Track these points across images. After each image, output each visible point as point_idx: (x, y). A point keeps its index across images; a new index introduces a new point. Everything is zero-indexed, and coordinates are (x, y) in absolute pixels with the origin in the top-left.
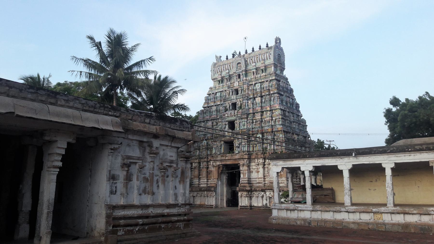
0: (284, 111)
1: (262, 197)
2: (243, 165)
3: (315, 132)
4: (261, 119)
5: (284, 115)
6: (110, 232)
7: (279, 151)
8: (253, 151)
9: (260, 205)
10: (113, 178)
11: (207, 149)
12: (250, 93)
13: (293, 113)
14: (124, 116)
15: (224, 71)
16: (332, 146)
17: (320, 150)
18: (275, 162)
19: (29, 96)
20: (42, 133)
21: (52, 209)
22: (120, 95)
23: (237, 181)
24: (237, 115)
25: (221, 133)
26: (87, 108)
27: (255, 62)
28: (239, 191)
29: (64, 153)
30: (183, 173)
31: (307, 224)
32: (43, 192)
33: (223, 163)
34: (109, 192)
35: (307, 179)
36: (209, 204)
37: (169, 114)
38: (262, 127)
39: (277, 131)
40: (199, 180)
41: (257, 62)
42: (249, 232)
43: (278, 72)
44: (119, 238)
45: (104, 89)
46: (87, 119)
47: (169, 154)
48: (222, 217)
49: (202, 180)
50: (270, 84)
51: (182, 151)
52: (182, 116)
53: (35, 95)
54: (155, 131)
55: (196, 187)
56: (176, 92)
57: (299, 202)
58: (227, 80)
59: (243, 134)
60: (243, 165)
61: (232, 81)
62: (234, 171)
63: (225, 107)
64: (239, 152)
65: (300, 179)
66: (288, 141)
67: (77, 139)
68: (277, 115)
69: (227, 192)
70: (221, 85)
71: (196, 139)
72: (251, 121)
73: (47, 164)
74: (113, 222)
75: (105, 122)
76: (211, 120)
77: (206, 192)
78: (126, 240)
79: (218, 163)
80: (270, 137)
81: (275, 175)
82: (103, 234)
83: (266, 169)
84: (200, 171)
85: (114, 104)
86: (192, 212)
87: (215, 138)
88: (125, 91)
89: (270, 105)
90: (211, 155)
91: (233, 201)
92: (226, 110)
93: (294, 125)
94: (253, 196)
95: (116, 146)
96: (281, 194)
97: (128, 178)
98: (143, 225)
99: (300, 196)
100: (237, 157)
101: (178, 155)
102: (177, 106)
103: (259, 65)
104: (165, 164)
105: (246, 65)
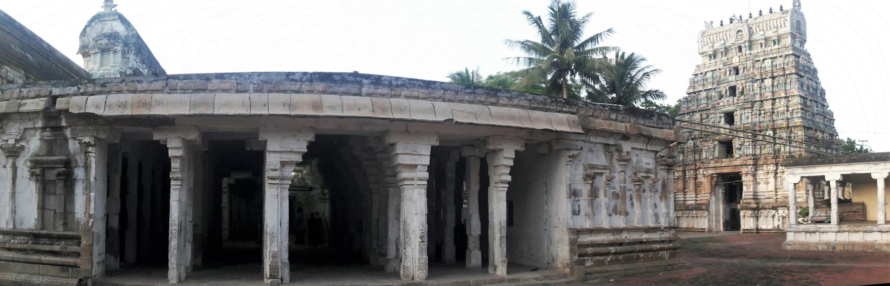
0: (804, 98)
1: (773, 216)
3: (844, 130)
5: (805, 104)
6: (575, 262)
7: (796, 155)
9: (770, 227)
10: (574, 194)
11: (695, 152)
12: (756, 72)
13: (817, 102)
14: (582, 112)
16: (865, 148)
17: (852, 153)
18: (791, 170)
19: (467, 98)
20: (484, 141)
21: (504, 234)
22: (570, 82)
23: (738, 195)
25: (713, 129)
26: (535, 105)
28: (742, 209)
29: (512, 164)
30: (664, 186)
31: (831, 249)
32: (492, 213)
33: (718, 172)
34: (569, 213)
35: (833, 191)
37: (639, 104)
39: (795, 127)
42: (756, 262)
43: (797, 45)
44: (588, 270)
45: (549, 77)
46: (537, 119)
47: (645, 160)
48: (718, 244)
50: (786, 61)
51: (662, 157)
52: (657, 106)
53: (473, 96)
54: (624, 130)
55: (681, 205)
56: (647, 74)
57: (821, 222)
61: (730, 56)
63: (720, 92)
64: (741, 156)
65: (823, 191)
66: (809, 140)
67: (526, 145)
69: (724, 211)
70: (713, 61)
71: (681, 140)
73: (494, 179)
74: (579, 251)
75: (559, 121)
78: (597, 272)
79: (711, 172)
80: (784, 135)
81: (792, 187)
82: (568, 265)
83: (779, 179)
84: (685, 182)
85: (565, 97)
86: (679, 238)
87: (705, 136)
88: (578, 78)
91: (733, 222)
92: (721, 97)
93: (818, 119)
95: (576, 153)
96: (799, 211)
97: (594, 194)
98: (615, 253)
99: (823, 214)
100: (738, 162)
101: (656, 162)
102: (649, 93)
103: (769, 34)
104: (640, 175)
105: (751, 34)
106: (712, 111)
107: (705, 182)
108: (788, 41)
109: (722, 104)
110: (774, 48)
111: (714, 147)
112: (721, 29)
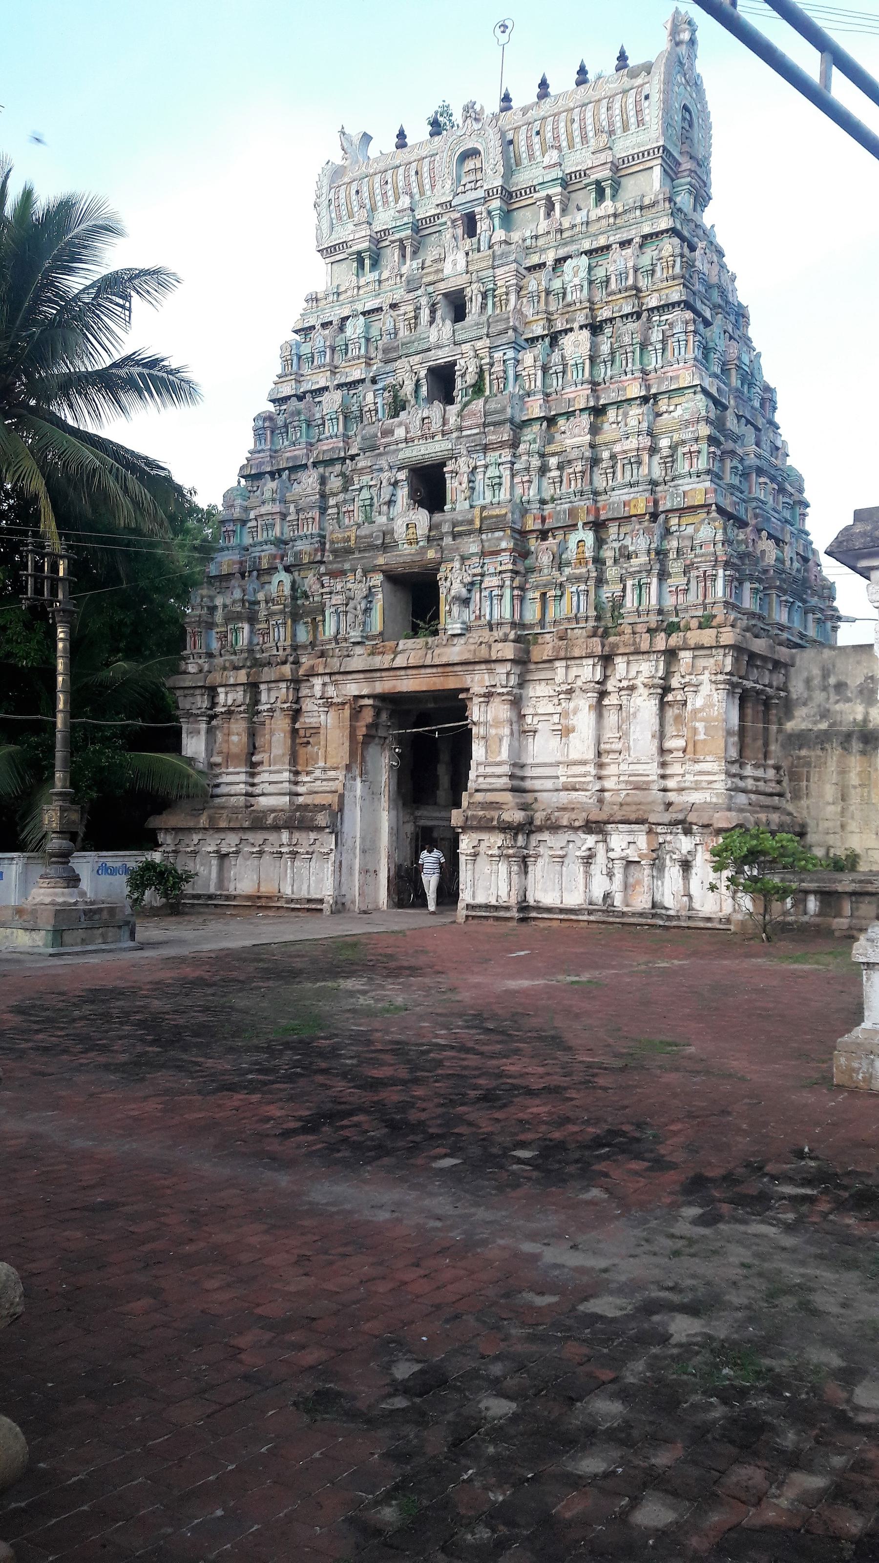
1: (588, 859)
2: (489, 696)
4: (592, 446)
5: (718, 424)
8: (542, 623)
9: (574, 899)
12: (528, 311)
15: (385, 203)
24: (460, 429)
27: (559, 148)
28: (465, 828)
33: (380, 687)
36: (304, 894)
38: (596, 493)
40: (253, 775)
41: (571, 146)
43: (684, 200)
49: (265, 777)
50: (645, 261)
55: (235, 810)
58: (403, 248)
59: (490, 524)
60: (489, 696)
61: (430, 254)
62: (435, 730)
63: (395, 390)
64: (468, 628)
68: (687, 423)
69: (396, 833)
70: (370, 276)
72: (536, 462)
76: (315, 465)
77: (285, 836)
79: (353, 688)
83: (611, 718)
89: (644, 372)
90: (313, 644)
92: (398, 406)
94: (537, 856)
100: (455, 652)
103: (579, 159)
105: (511, 165)
106: (362, 463)
107: (332, 729)
108: (652, 182)
109: (400, 433)
110: (596, 213)
111: (369, 596)
112: (403, 156)
